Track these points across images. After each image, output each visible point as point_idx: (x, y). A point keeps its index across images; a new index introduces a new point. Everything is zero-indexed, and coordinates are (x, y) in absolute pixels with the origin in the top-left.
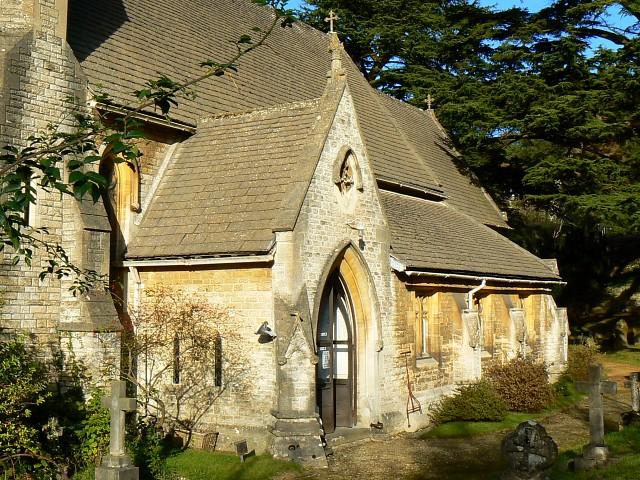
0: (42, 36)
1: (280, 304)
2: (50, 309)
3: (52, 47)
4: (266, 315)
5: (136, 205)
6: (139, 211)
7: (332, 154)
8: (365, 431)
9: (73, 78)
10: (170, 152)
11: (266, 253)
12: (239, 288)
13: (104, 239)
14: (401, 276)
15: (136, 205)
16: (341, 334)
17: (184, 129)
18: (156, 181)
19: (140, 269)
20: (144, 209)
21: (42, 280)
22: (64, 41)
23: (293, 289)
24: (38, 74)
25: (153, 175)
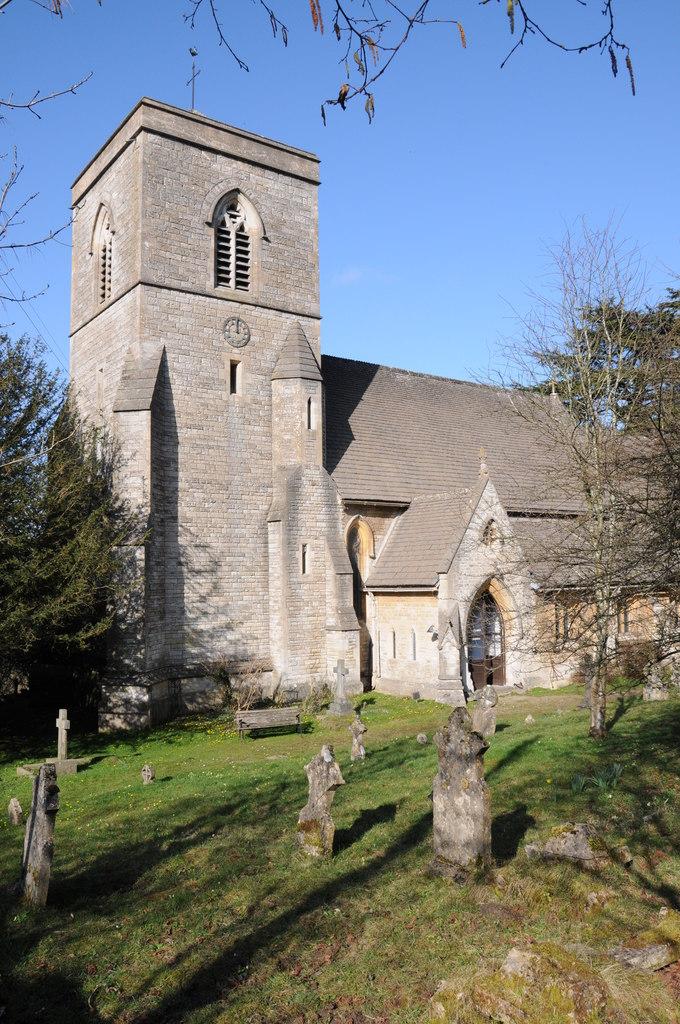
0: (307, 467)
1: (441, 615)
2: (319, 618)
3: (315, 469)
4: (435, 622)
5: (372, 554)
6: (374, 558)
7: (479, 522)
8: (510, 688)
9: (328, 487)
10: (393, 523)
11: (434, 586)
12: (423, 605)
13: (349, 579)
14: (536, 592)
15: (372, 554)
16: (497, 629)
17: (402, 505)
18: (385, 540)
19: (375, 594)
20: (377, 557)
21: (619, 699)
22: (321, 466)
23: (448, 606)
24: (307, 488)
25: (384, 535)
